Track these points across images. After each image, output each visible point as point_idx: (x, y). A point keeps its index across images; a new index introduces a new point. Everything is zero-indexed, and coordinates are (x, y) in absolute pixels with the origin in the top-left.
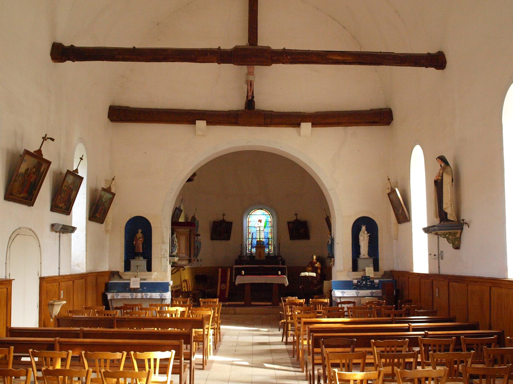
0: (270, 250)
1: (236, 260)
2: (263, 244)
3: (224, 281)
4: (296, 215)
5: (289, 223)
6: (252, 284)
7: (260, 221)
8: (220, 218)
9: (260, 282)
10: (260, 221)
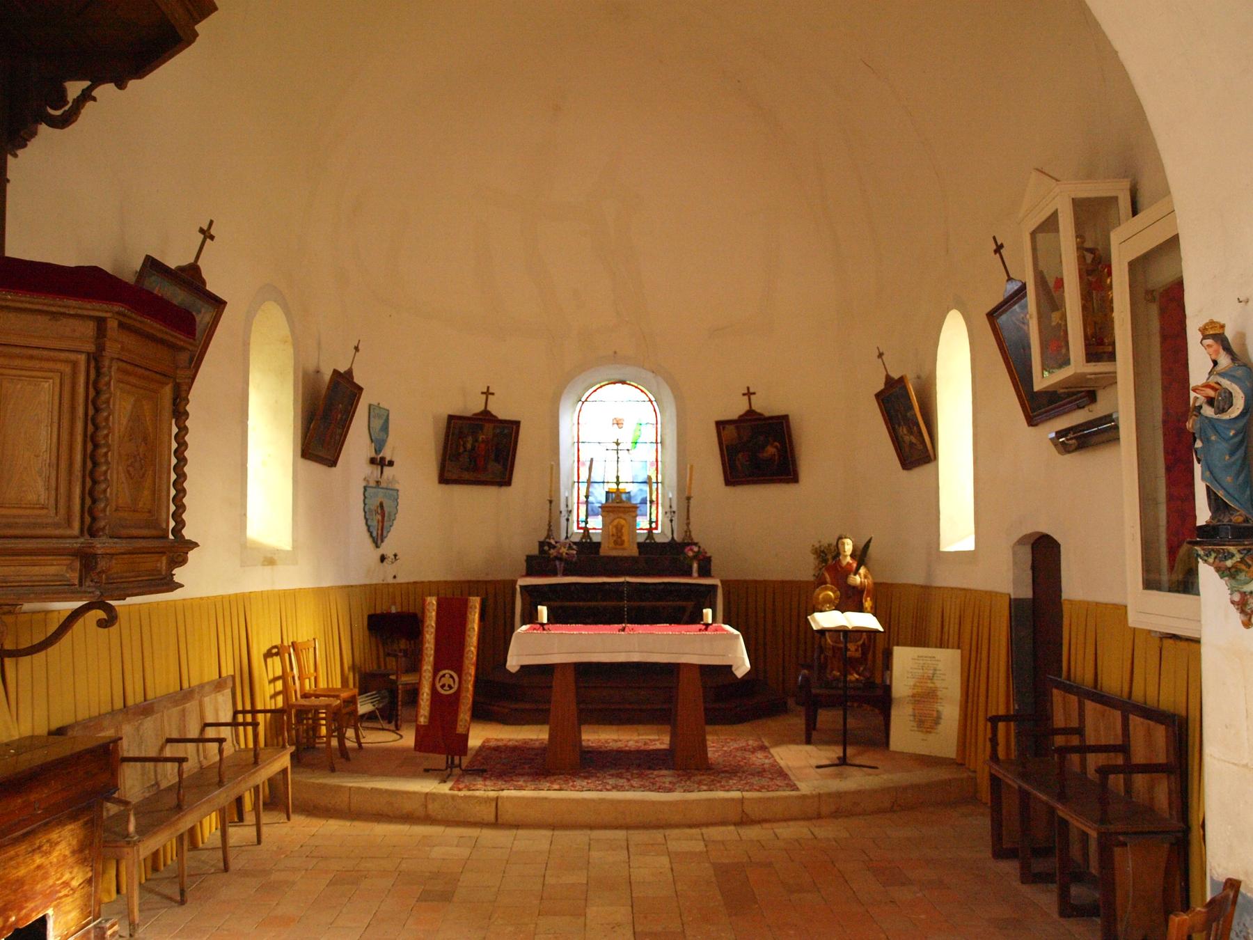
0: (651, 522)
1: (530, 559)
2: (629, 498)
3: (450, 656)
4: (749, 394)
5: (720, 425)
6: (584, 670)
7: (618, 423)
8: (475, 406)
9: (621, 658)
10: (618, 423)
